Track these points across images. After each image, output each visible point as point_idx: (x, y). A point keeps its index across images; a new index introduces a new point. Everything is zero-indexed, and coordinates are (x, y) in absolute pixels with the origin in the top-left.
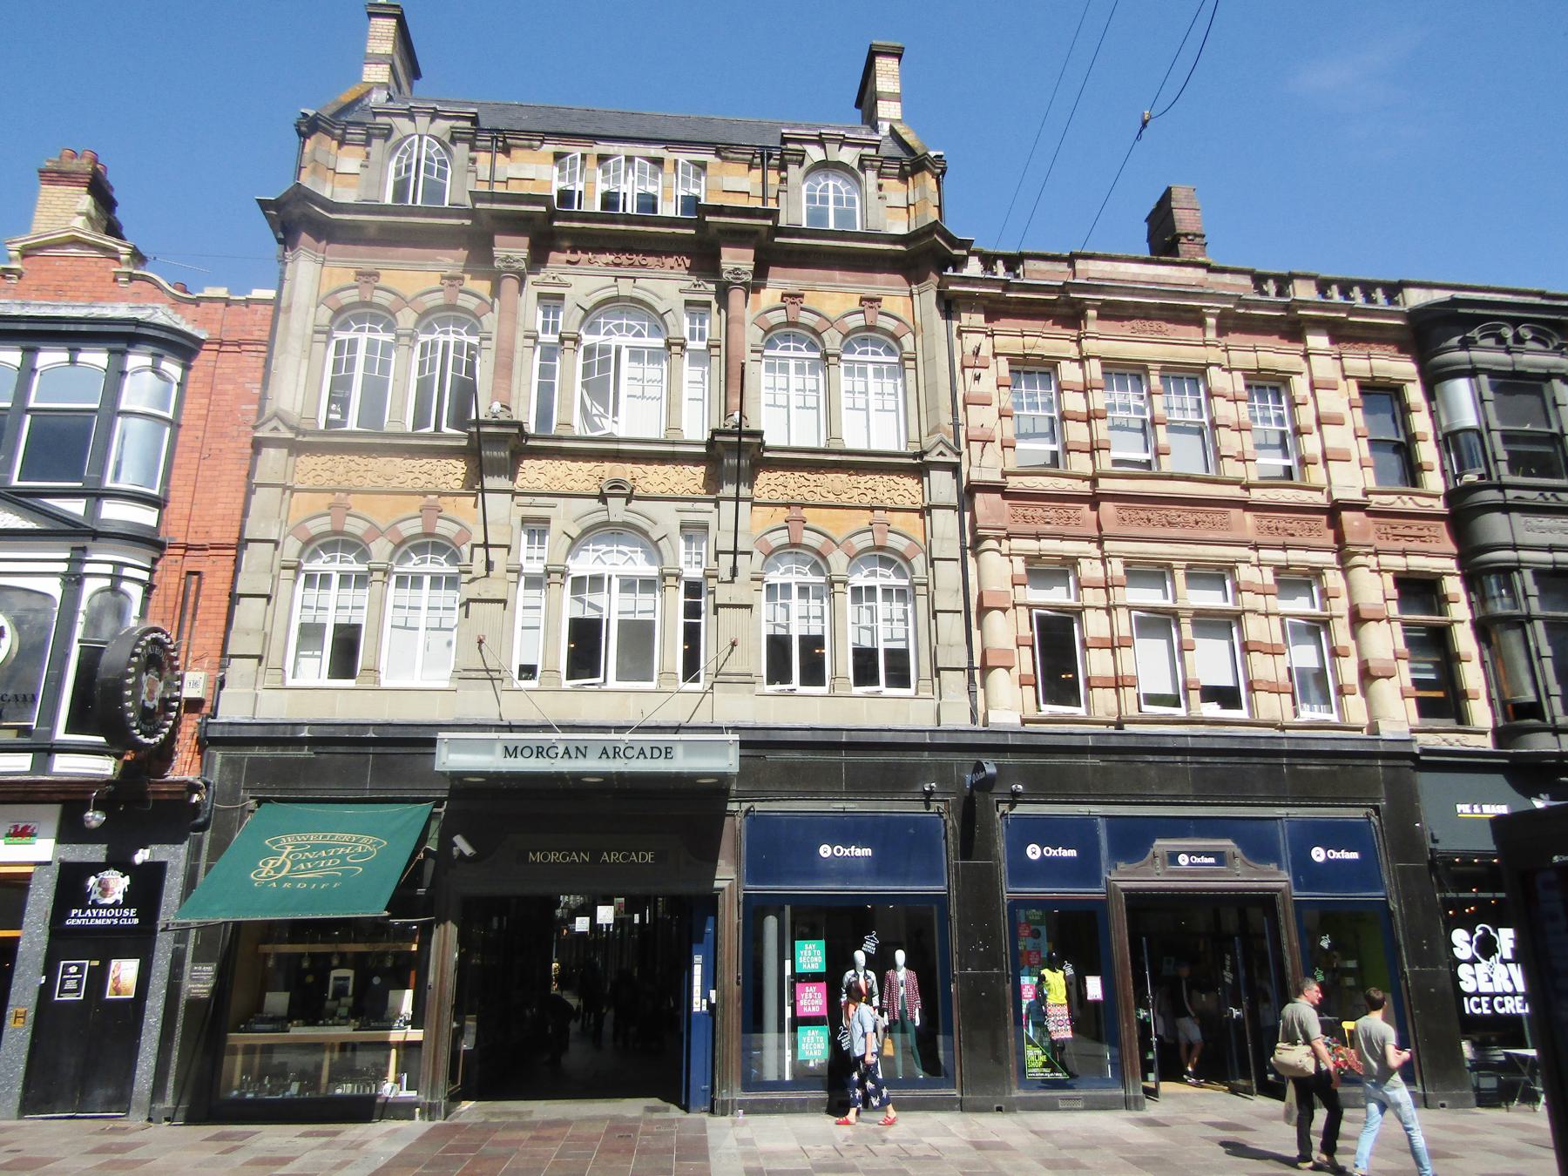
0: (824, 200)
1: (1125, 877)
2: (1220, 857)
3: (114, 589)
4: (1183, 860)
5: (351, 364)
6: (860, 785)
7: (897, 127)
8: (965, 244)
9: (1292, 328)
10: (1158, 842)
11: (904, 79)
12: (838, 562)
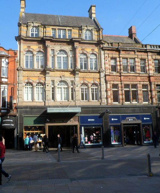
0: (87, 35)
1: (123, 122)
2: (134, 119)
3: (4, 90)
4: (130, 120)
5: (28, 59)
6: (93, 113)
7: (95, 19)
8: (105, 42)
9: (146, 52)
10: (127, 118)
11: (96, 10)
12: (90, 85)
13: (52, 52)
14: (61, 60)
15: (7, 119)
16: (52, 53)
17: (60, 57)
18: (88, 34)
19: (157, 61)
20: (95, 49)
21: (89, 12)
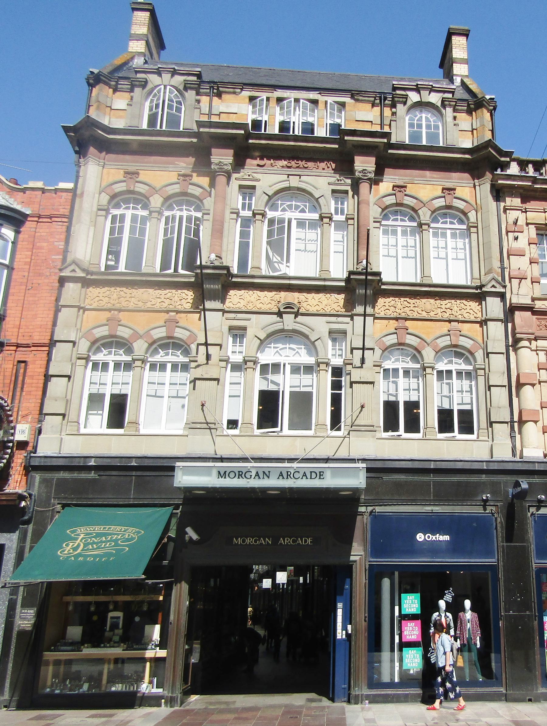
0: (420, 126)
5: (121, 229)
8: (508, 154)
18: (424, 123)
21: (441, 66)
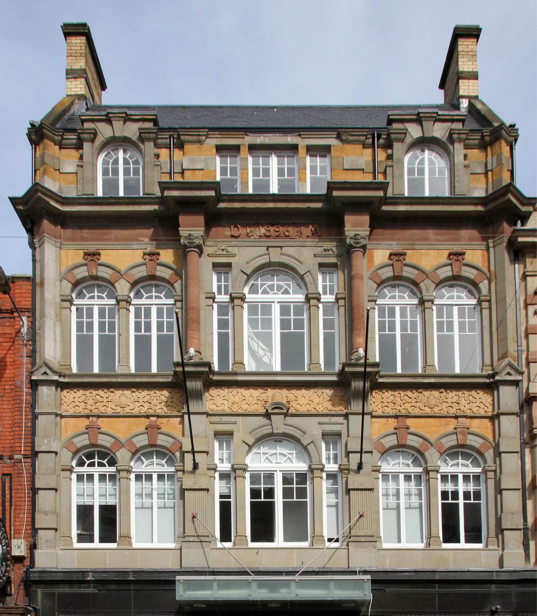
13: (219, 280)
14: (268, 323)
15: (328, 449)
16: (219, 287)
17: (267, 308)
19: (29, 543)
20: (468, 253)
